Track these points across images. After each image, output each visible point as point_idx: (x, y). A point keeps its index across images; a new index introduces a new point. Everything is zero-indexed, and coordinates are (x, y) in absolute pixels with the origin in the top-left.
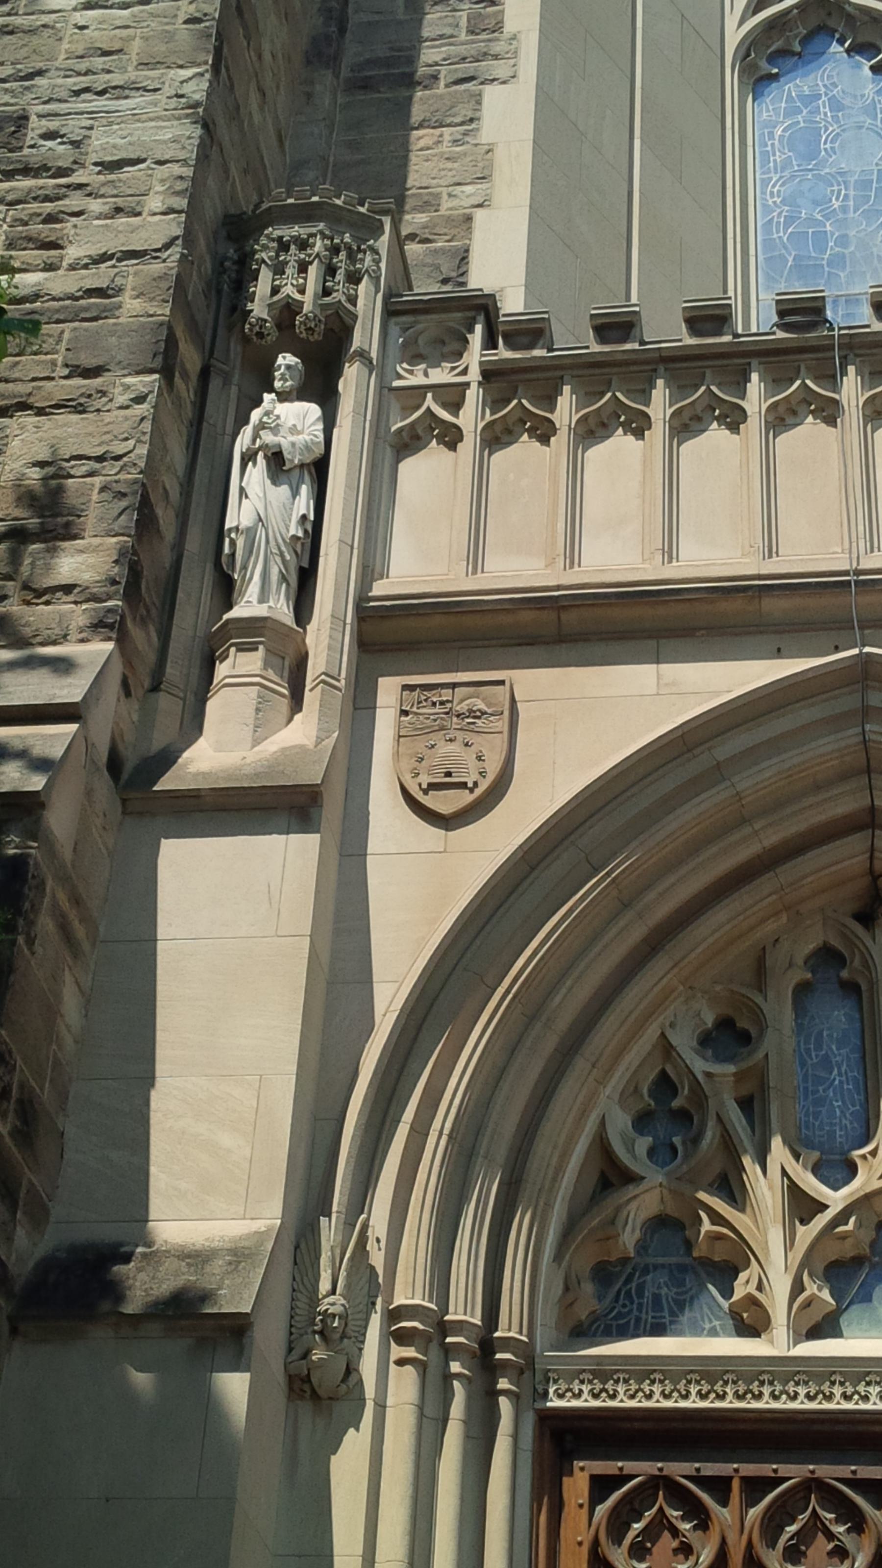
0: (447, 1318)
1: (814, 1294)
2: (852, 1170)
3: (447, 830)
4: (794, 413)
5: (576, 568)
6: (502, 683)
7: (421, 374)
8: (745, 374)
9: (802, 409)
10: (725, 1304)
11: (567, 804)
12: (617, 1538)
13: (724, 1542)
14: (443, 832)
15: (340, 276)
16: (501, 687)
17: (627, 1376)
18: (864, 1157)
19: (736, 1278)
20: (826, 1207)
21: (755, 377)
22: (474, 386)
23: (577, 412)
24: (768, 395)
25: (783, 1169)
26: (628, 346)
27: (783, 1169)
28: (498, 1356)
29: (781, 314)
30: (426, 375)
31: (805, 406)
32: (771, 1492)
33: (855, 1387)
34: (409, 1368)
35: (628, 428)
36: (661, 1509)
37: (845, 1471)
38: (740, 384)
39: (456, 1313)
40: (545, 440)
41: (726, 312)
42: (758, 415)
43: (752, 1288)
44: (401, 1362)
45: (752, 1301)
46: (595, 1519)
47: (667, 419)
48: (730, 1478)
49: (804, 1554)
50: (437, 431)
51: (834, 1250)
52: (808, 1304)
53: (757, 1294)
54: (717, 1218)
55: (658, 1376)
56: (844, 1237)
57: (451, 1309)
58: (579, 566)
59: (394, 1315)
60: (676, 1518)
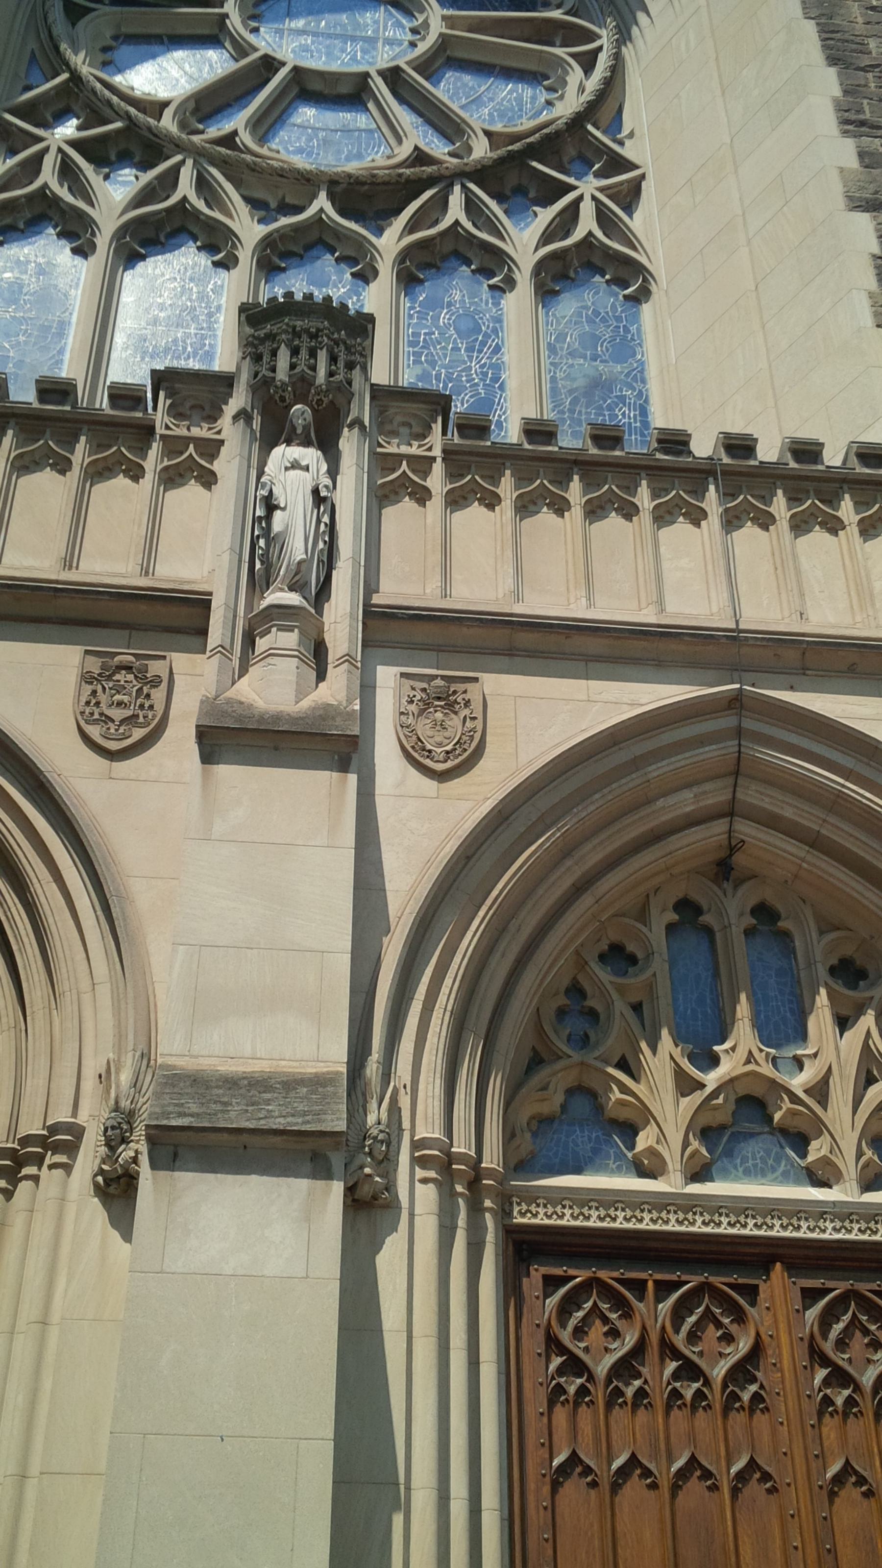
0: (453, 1150)
3: (112, 761)
6: (164, 657)
7: (395, 446)
8: (568, 474)
9: (609, 506)
10: (630, 1155)
11: (532, 775)
13: (644, 1328)
14: (109, 762)
15: (341, 364)
16: (162, 662)
18: (726, 1051)
21: (83, 439)
22: (439, 460)
23: (16, 449)
24: (655, 495)
25: (671, 1055)
26: (550, 448)
27: (671, 1055)
28: (484, 1182)
30: (189, 429)
31: (677, 509)
34: (431, 1186)
35: (126, 473)
37: (616, 1274)
38: (70, 443)
39: (459, 1147)
40: (697, 523)
41: (487, 424)
43: (652, 1142)
44: (424, 1181)
47: (85, 465)
48: (646, 1281)
51: (706, 1119)
52: (866, 1165)
53: (656, 1146)
54: (624, 1089)
55: (699, 1209)
56: (716, 1108)
57: (455, 1143)
59: (416, 1145)
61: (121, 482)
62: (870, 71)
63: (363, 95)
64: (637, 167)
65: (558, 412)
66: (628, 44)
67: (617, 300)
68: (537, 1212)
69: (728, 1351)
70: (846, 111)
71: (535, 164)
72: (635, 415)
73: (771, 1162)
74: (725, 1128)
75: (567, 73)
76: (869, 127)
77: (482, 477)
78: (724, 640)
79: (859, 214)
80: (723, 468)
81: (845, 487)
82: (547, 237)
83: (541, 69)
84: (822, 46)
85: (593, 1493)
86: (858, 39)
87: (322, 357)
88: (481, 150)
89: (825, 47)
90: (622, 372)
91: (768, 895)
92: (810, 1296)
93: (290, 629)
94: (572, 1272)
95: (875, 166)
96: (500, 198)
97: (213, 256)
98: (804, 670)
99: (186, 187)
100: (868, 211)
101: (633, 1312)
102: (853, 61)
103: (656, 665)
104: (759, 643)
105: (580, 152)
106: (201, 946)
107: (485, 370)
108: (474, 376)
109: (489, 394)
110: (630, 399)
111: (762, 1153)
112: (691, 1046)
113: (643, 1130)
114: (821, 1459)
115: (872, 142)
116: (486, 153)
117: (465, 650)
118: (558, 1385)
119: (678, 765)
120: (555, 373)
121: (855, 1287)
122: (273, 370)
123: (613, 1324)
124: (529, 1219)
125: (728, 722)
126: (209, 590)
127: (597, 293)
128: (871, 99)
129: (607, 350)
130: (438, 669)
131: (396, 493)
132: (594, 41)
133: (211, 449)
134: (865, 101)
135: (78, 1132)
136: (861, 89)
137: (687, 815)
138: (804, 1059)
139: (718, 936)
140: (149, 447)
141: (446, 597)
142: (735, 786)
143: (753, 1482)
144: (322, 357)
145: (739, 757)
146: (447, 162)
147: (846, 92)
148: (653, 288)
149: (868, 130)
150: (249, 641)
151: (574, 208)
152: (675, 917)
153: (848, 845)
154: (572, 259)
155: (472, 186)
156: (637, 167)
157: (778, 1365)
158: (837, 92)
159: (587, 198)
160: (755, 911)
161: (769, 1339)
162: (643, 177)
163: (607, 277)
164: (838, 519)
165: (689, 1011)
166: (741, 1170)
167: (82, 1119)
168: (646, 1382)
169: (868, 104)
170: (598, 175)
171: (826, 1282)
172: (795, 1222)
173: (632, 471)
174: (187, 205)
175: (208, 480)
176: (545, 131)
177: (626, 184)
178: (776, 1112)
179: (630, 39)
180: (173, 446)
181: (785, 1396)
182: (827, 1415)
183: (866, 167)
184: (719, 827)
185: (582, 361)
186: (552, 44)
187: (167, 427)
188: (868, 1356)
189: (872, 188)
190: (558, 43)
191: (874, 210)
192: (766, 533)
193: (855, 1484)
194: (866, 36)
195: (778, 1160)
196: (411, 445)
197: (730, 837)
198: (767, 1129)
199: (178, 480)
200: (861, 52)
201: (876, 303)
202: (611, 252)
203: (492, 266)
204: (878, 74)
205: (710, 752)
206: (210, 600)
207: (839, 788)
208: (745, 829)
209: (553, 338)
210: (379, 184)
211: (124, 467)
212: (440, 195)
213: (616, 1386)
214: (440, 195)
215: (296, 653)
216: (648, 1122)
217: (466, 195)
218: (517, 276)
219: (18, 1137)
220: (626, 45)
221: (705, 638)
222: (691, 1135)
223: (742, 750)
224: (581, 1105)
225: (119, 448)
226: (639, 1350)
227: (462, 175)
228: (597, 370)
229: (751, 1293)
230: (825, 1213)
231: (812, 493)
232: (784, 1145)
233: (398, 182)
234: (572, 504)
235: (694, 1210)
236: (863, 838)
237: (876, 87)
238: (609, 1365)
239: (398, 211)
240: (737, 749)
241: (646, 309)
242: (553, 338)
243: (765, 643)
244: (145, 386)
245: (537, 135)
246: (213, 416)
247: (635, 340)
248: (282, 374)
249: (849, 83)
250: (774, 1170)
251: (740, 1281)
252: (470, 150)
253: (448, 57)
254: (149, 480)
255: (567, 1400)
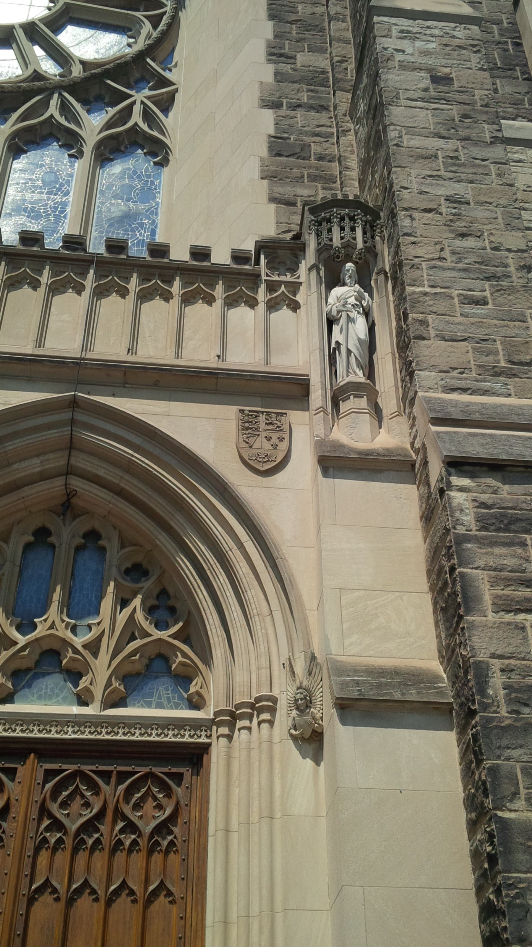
1: (116, 687)
2: (34, 627)
4: (194, 298)
5: (269, 365)
12: (127, 800)
13: (105, 801)
17: (22, 723)
19: (191, 683)
20: (17, 643)
24: (183, 287)
29: (64, 242)
32: (131, 778)
33: (195, 732)
35: (247, 303)
36: (77, 786)
38: (84, 274)
40: (79, 293)
42: (134, 292)
45: (87, 689)
46: (118, 793)
47: (137, 291)
49: (142, 807)
50: (202, 295)
51: (128, 668)
54: (185, 655)
56: (134, 662)
58: (93, 351)
60: (84, 790)
61: (26, 290)
62: (295, 24)
63: (10, 39)
64: (174, 84)
65: (99, 233)
66: (183, 10)
67: (149, 165)
68: (185, 734)
69: (157, 815)
70: (273, 48)
71: (109, 82)
72: (148, 235)
73: (56, 691)
74: (31, 670)
75: (141, 27)
76: (285, 58)
77: (246, 288)
78: (72, 365)
79: (266, 110)
80: (98, 259)
81: (178, 272)
82: (108, 125)
83: (128, 25)
84: (268, 8)
85: (95, 905)
86: (291, 5)
87: (336, 230)
88: (77, 71)
89: (269, 9)
90: (144, 209)
91: (97, 525)
92: (49, 774)
93: (361, 397)
94: (137, 769)
95: (283, 81)
96: (84, 102)
97: (69, 151)
98: (125, 384)
99: (137, 118)
100: (272, 109)
101: (172, 793)
102: (285, 17)
103: (28, 380)
104: (94, 367)
105: (143, 75)
106: (340, 589)
107: (56, 205)
108: (49, 209)
109: (57, 220)
110: (146, 225)
111: (52, 685)
112: (19, 619)
113: (85, 676)
114: (185, 881)
115: (285, 66)
116: (80, 73)
117: (109, 384)
118: (119, 839)
119: (27, 442)
120: (102, 208)
121: (153, 771)
122: (331, 240)
123: (159, 801)
124: (129, 737)
125: (66, 415)
126: (308, 373)
127: (137, 161)
128: (291, 41)
129: (138, 194)
130: (262, 408)
131: (194, 298)
132: (163, 8)
133: (295, 287)
134: (287, 42)
135: (274, 700)
136: (286, 34)
137: (97, 476)
138: (92, 626)
139: (57, 549)
140: (258, 287)
141: (267, 364)
142: (69, 455)
143: (124, 895)
144: (336, 230)
145: (71, 437)
146: (51, 79)
147: (276, 36)
148: (171, 158)
149: (284, 59)
150: (336, 404)
151: (129, 109)
152: (32, 539)
153: (135, 493)
154: (124, 139)
155: (66, 94)
156: (174, 84)
157: (16, 818)
158: (270, 35)
159: (138, 103)
160: (85, 536)
161: (15, 802)
162: (177, 90)
163: (145, 151)
164: (170, 293)
165: (29, 597)
166: (36, 696)
167: (276, 692)
168: (175, 837)
169: (288, 43)
170: (151, 89)
171: (63, 765)
172: (48, 728)
173: (41, 260)
174: (53, 120)
175: (295, 306)
176: (117, 62)
177: (165, 95)
178: (64, 660)
179: (185, 8)
180: (272, 287)
181: (15, 839)
182: (44, 849)
183: (277, 82)
184: (59, 482)
185: (120, 201)
186: (138, 10)
187: (267, 275)
188: (154, 814)
189: (278, 94)
190: (141, 10)
191: (277, 108)
192: (295, 314)
193: (89, 894)
194: (297, 3)
195: (61, 690)
196: (286, 275)
197: (66, 488)
198: (58, 670)
199: (192, 300)
200: (292, 12)
201: (264, 164)
202: (147, 135)
203: (72, 143)
204: (298, 26)
205: (53, 433)
206: (309, 380)
207: (130, 457)
208: (76, 483)
209: (104, 187)
210: (6, 92)
211: (28, 281)
212: (45, 99)
213: (157, 840)
214: (45, 99)
215: (367, 411)
216: (198, 675)
217: (62, 100)
218: (85, 149)
219: (235, 703)
220: (182, 11)
221: (59, 363)
222: (113, 678)
223: (73, 433)
224: (158, 664)
225: (241, 288)
226: (101, 815)
227: (59, 87)
228: (129, 207)
229: (178, 778)
230: (69, 722)
231: (157, 276)
232: (66, 680)
233: (18, 92)
234: (216, 298)
235: (102, 725)
236: (144, 489)
237: (296, 33)
238: (154, 826)
239: (15, 110)
240: (70, 433)
241: (166, 171)
242: (104, 187)
243: (98, 367)
244: (251, 251)
245: (112, 64)
246: (294, 269)
247: (157, 190)
248: (336, 242)
249: (279, 30)
250: (58, 695)
251: (7, 765)
252: (71, 72)
253: (70, 17)
254: (86, 294)
255: (49, 847)
